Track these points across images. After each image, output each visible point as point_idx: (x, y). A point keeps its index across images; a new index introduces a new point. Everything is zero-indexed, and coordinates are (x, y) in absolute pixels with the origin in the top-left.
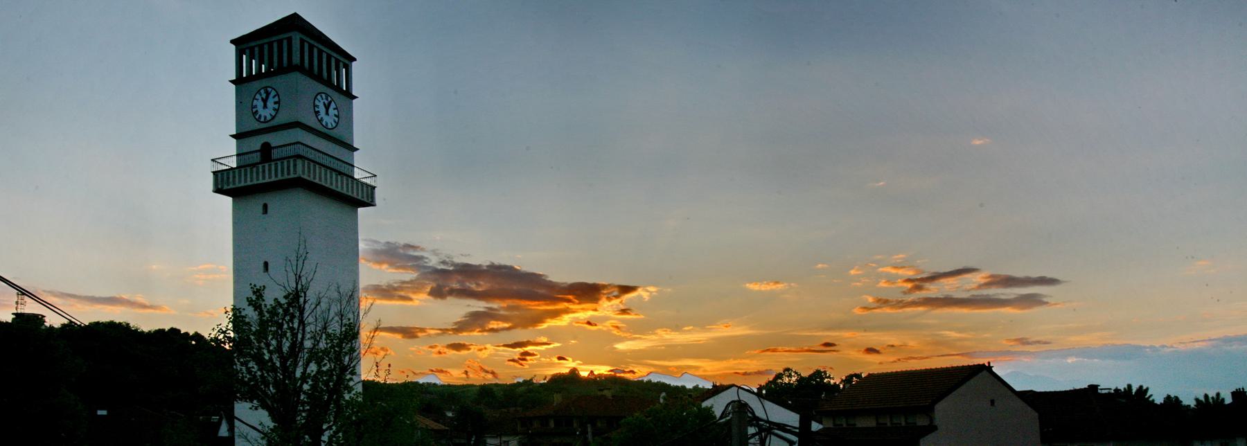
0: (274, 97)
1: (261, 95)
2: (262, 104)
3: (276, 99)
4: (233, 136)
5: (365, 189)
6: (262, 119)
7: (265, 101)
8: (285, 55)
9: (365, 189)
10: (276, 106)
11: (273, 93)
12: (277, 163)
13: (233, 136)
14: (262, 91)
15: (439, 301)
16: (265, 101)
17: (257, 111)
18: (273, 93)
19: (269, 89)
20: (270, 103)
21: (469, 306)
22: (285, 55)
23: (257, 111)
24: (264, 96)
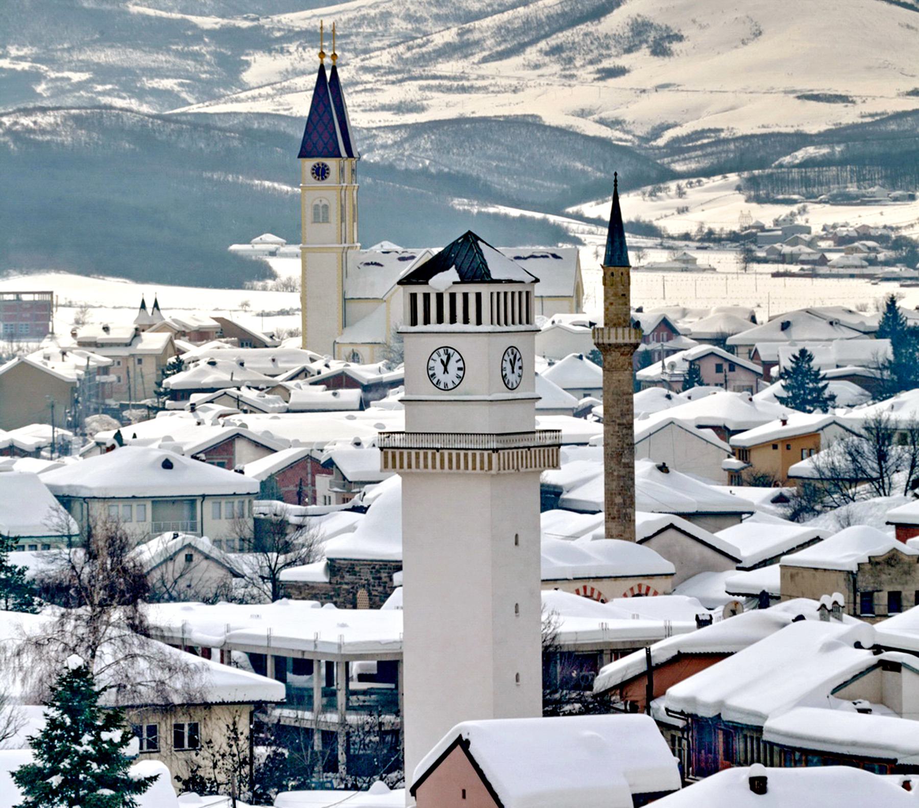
0: (457, 361)
1: (439, 356)
2: (442, 368)
3: (460, 364)
4: (13, 774)
5: (762, 758)
6: (442, 386)
7: (445, 365)
8: (755, 747)
9: (762, 758)
10: (461, 373)
11: (457, 357)
12: (243, 502)
13: (13, 774)
14: (442, 351)
15: (656, 58)
16: (445, 365)
17: (434, 374)
18: (456, 357)
19: (451, 351)
20: (453, 366)
21: (448, 105)
22: (755, 747)
23: (434, 374)
24: (445, 358)
